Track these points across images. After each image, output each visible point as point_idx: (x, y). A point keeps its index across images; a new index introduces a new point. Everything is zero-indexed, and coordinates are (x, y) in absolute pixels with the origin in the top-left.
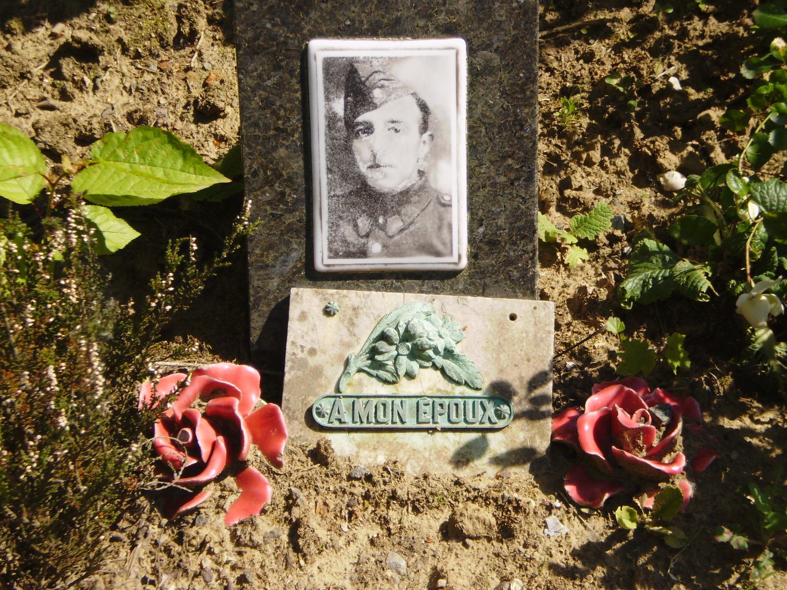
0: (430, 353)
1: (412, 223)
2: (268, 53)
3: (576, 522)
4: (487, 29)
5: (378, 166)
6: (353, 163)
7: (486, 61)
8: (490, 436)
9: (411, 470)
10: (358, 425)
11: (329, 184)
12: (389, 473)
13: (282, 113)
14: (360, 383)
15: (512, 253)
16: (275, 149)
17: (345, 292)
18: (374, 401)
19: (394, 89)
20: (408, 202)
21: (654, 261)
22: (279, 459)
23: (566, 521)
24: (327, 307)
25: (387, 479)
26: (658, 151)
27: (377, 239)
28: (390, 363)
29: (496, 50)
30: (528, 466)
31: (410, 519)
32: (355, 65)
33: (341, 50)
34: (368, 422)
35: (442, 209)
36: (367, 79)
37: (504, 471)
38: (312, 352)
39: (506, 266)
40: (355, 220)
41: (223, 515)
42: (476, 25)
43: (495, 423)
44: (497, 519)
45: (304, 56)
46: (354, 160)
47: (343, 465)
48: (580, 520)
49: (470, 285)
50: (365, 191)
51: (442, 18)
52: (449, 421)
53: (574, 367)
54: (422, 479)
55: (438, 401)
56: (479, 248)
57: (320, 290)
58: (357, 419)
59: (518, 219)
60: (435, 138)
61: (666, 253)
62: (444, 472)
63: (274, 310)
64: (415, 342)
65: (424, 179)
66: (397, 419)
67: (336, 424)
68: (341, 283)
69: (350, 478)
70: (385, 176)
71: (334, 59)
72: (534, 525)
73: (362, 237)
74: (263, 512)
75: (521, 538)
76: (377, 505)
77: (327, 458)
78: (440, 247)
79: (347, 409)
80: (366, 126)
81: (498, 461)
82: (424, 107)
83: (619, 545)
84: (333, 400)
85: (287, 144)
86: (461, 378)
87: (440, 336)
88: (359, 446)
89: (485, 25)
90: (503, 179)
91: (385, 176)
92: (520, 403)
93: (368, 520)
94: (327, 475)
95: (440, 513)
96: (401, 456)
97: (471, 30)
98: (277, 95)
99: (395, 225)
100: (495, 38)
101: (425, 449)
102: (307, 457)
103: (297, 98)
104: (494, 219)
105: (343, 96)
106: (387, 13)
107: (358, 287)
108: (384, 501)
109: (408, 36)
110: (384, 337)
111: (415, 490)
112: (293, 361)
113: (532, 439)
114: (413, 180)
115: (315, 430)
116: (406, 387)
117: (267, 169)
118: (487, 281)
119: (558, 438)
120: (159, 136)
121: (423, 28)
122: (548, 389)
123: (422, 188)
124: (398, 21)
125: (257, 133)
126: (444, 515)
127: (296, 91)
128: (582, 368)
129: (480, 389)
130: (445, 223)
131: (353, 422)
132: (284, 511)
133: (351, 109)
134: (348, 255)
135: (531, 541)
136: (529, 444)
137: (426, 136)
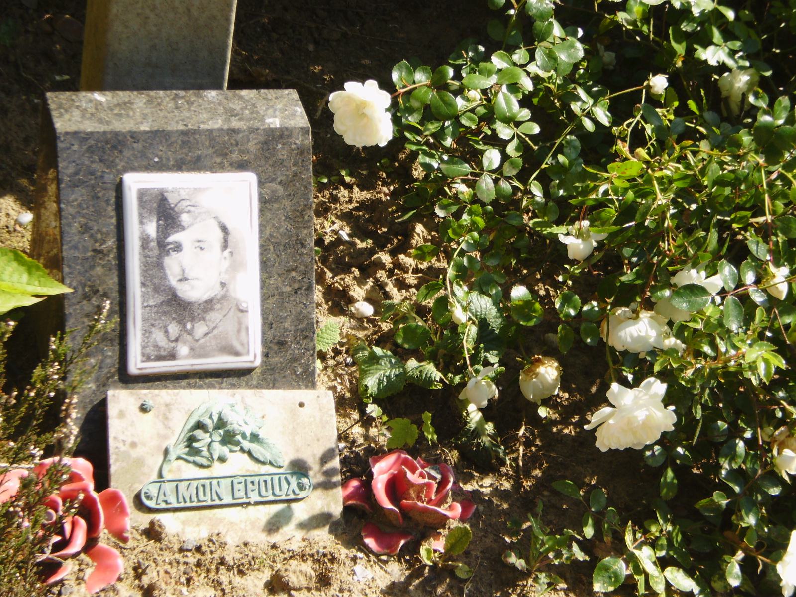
0: (239, 438)
1: (215, 328)
2: (87, 186)
3: (377, 568)
4: (273, 166)
5: (186, 279)
6: (164, 277)
7: (272, 191)
8: (294, 506)
9: (232, 540)
10: (182, 505)
11: (144, 295)
12: (214, 544)
13: (99, 236)
14: (179, 469)
15: (296, 352)
16: (92, 267)
17: (157, 391)
18: (195, 483)
19: (200, 213)
20: (212, 309)
21: (383, 364)
22: (126, 535)
23: (369, 568)
24: (143, 405)
25: (213, 549)
26: (348, 286)
27: (185, 343)
28: (205, 449)
29: (280, 183)
30: (327, 528)
31: (237, 580)
32: (165, 194)
33: (145, 182)
34: (191, 501)
35: (240, 315)
36: (176, 206)
37: (309, 534)
38: (134, 445)
39: (292, 363)
40: (165, 327)
41: (83, 585)
42: (263, 162)
43: (298, 494)
44: (315, 571)
45: (119, 188)
46: (165, 274)
47: (174, 540)
48: (380, 566)
49: (262, 380)
50: (175, 301)
51: (235, 156)
52: (260, 495)
53: (345, 447)
54: (243, 547)
55: (249, 479)
56: (270, 348)
57: (134, 391)
58: (181, 499)
59: (301, 322)
60: (234, 255)
61: (390, 357)
62: (260, 540)
63: (89, 412)
64: (226, 429)
65: (225, 289)
66: (215, 497)
67: (163, 506)
68: (150, 384)
69: (181, 550)
70: (193, 287)
71: (147, 190)
72: (344, 574)
73: (172, 342)
74: (120, 579)
75: (335, 586)
76: (208, 571)
77: (161, 534)
78: (239, 348)
79: (172, 491)
80: (176, 245)
81: (303, 526)
82: (224, 229)
83: (417, 581)
84: (159, 484)
85: (103, 263)
86: (266, 458)
87: (246, 423)
88: (184, 523)
89: (270, 162)
90: (288, 289)
91: (193, 287)
92: (315, 475)
93: (203, 584)
94: (161, 549)
95: (261, 574)
96: (222, 529)
97: (259, 166)
98: (95, 221)
99: (200, 329)
100: (279, 173)
101: (241, 521)
102: (141, 535)
103: (112, 224)
104: (282, 323)
105: (155, 220)
106: (190, 151)
107: (166, 387)
108: (213, 567)
109: (207, 170)
110: (199, 426)
111: (239, 556)
112: (117, 454)
113: (328, 505)
114: (216, 291)
115: (144, 512)
116: (218, 469)
117: (85, 285)
118: (277, 375)
119: (350, 502)
120: (6, 255)
121: (220, 164)
122: (336, 463)
123: (224, 297)
124: (199, 158)
125: (77, 254)
126: (266, 575)
127: (111, 217)
128: (350, 448)
129: (282, 467)
130: (243, 326)
131: (178, 502)
132: (135, 580)
133: (162, 231)
134: (159, 358)
135: (345, 586)
136: (326, 510)
137: (226, 253)
